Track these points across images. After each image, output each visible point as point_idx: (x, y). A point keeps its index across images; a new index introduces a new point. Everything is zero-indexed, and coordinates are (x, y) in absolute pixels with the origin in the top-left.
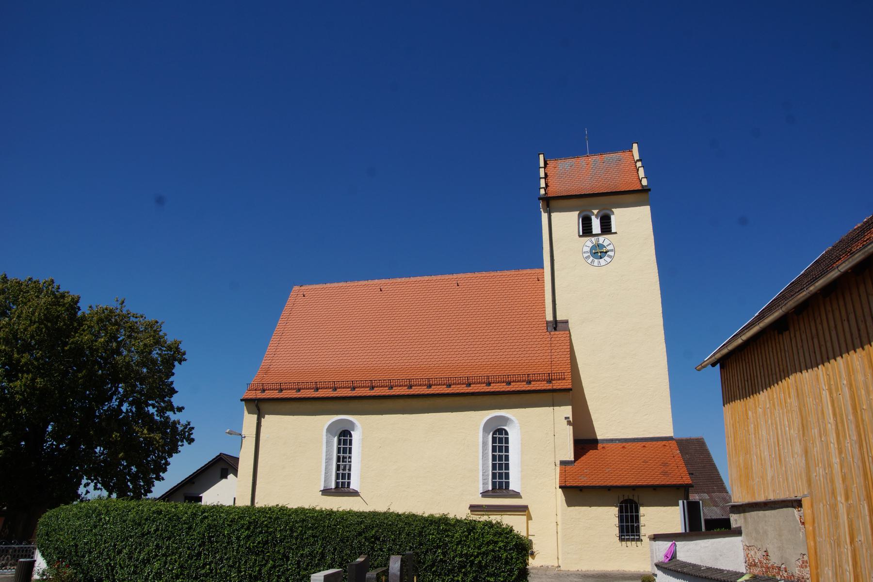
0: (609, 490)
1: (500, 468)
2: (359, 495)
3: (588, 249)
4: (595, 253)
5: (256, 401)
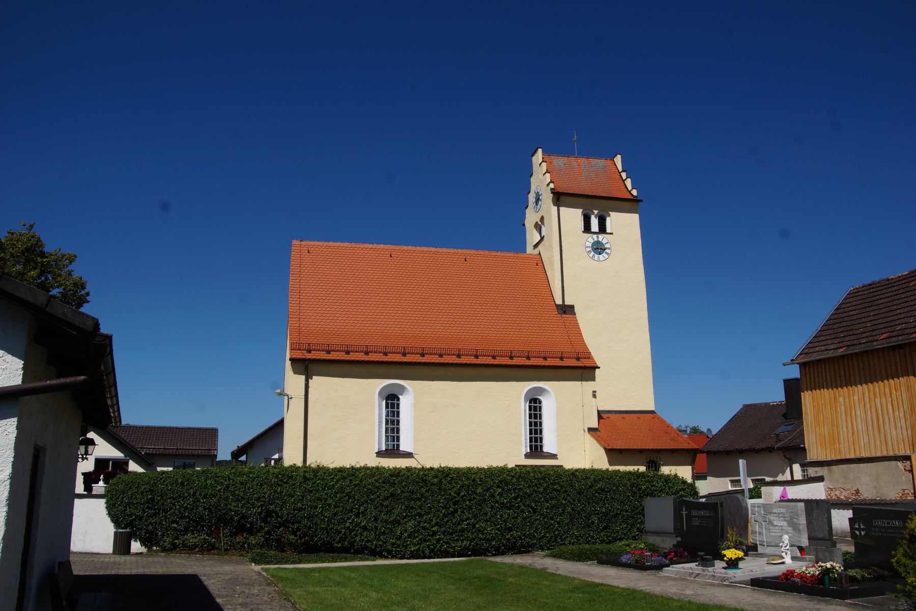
1: (536, 433)
2: (413, 457)
3: (590, 245)
4: (595, 249)
5: (307, 362)
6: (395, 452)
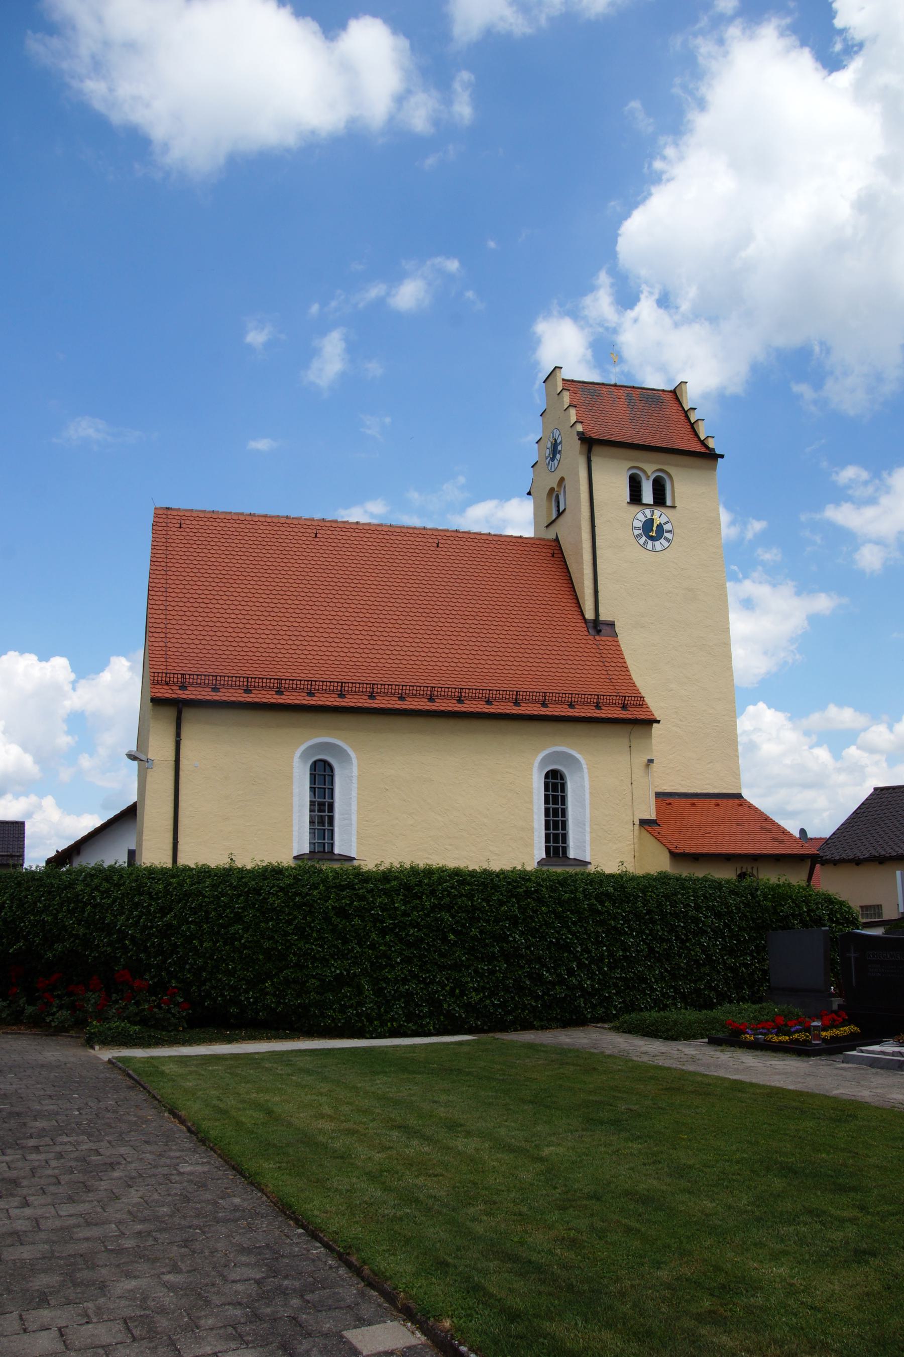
0: (857, 864)
3: (640, 525)
6: (326, 856)
